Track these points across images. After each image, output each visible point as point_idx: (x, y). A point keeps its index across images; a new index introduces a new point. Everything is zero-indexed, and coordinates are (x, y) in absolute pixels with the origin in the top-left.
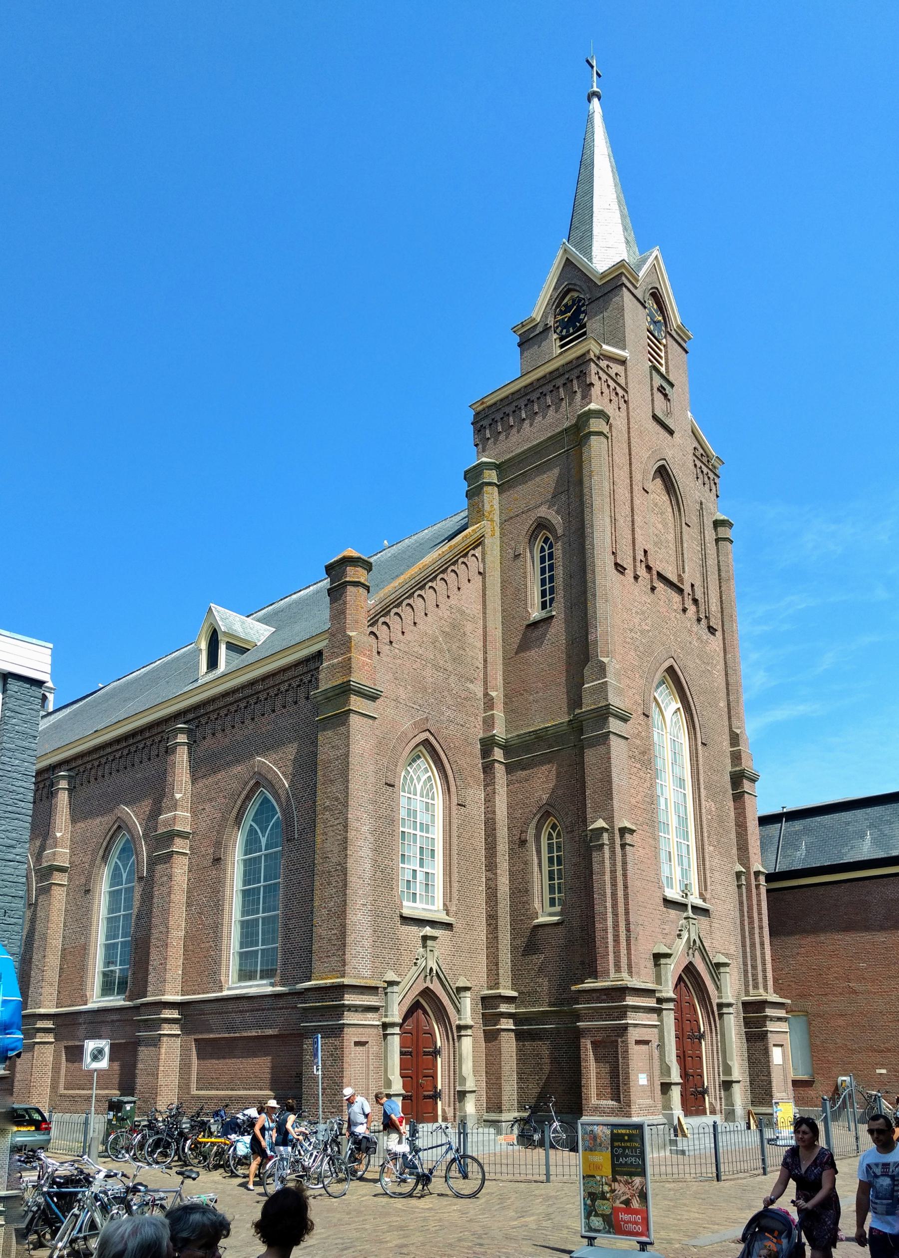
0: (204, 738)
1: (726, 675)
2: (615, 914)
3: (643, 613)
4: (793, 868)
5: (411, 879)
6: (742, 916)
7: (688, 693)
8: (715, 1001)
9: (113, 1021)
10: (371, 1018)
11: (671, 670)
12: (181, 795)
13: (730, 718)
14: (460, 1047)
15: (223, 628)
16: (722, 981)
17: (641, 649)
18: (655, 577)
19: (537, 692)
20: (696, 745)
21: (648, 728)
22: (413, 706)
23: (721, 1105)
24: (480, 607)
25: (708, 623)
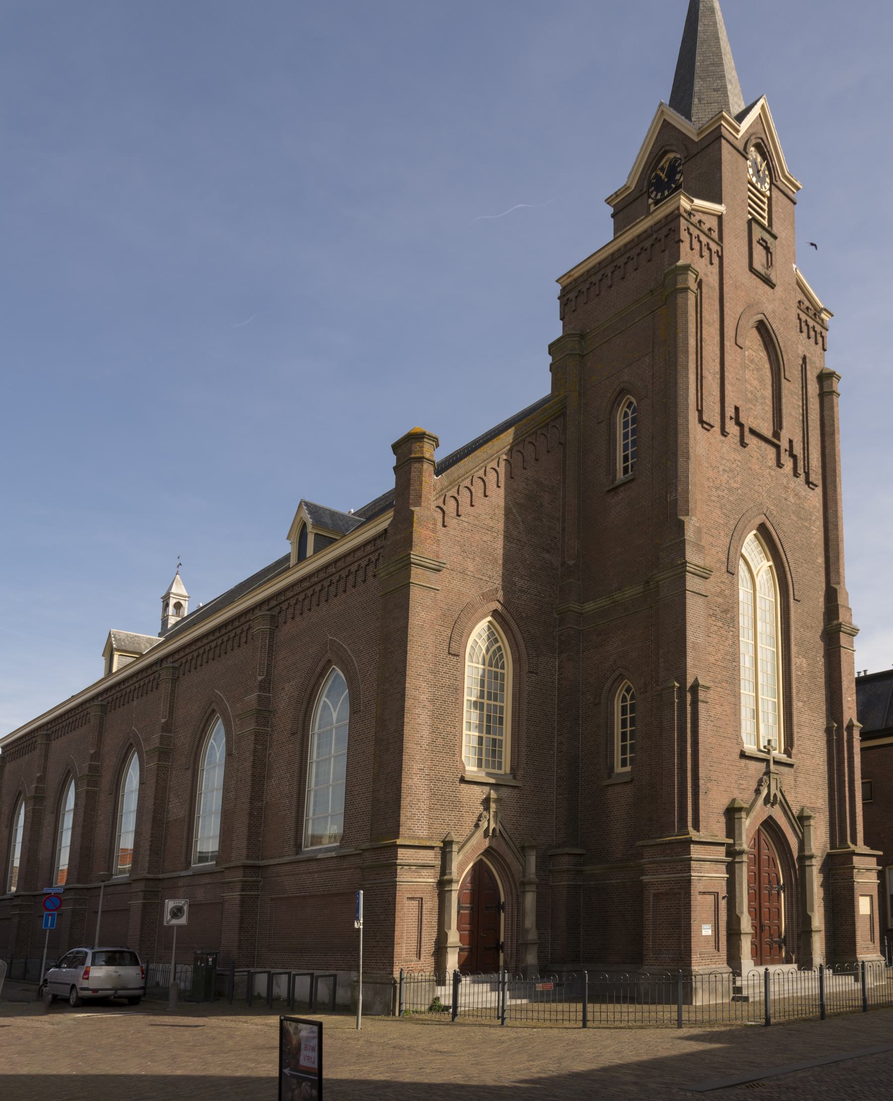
0: (285, 623)
3: (731, 470)
9: (205, 884)
22: (482, 577)
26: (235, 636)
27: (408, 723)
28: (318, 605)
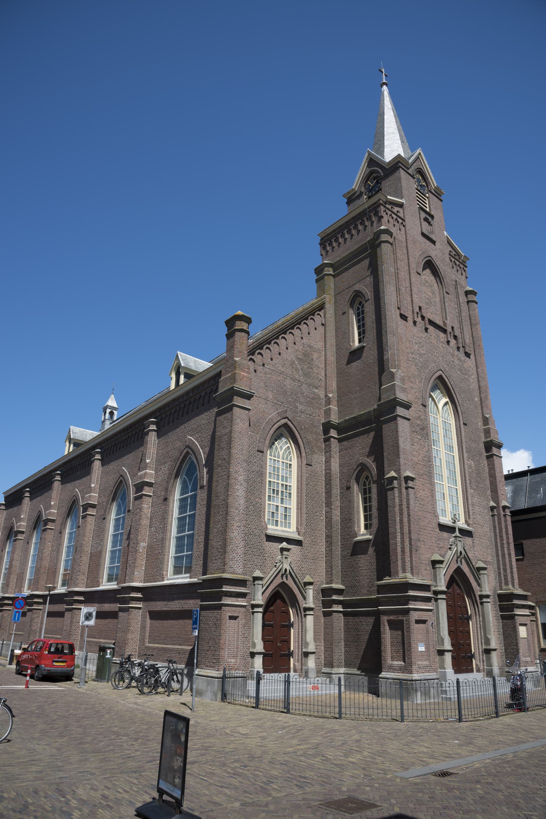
0: (164, 426)
1: (479, 381)
2: (402, 534)
3: (420, 343)
4: (536, 506)
5: (275, 512)
6: (496, 536)
7: (453, 392)
8: (478, 593)
10: (241, 600)
11: (440, 378)
12: (149, 460)
13: (482, 408)
14: (305, 622)
15: (183, 365)
16: (482, 579)
17: (419, 364)
18: (427, 322)
19: (356, 393)
20: (460, 424)
21: (426, 414)
22: (277, 402)
23: (483, 666)
24: (322, 344)
25: (465, 350)
26: (136, 434)
27: (230, 495)
28: (182, 416)
